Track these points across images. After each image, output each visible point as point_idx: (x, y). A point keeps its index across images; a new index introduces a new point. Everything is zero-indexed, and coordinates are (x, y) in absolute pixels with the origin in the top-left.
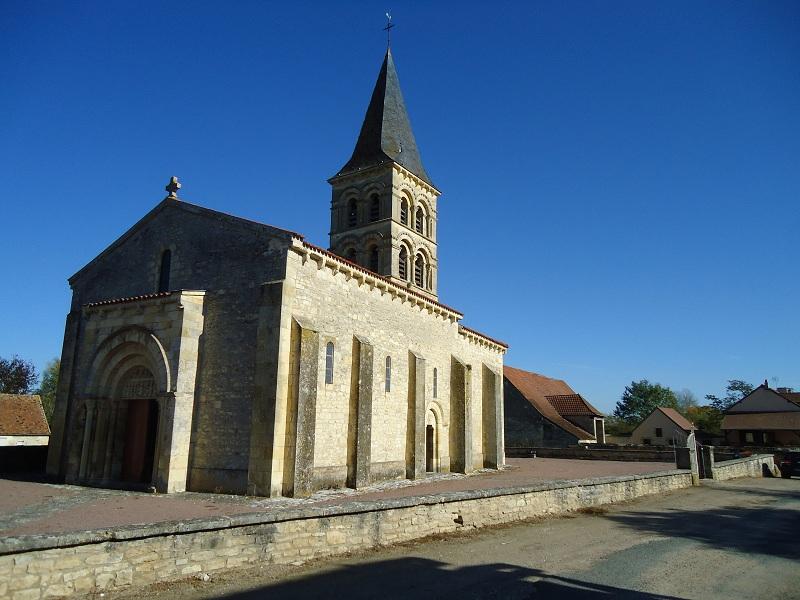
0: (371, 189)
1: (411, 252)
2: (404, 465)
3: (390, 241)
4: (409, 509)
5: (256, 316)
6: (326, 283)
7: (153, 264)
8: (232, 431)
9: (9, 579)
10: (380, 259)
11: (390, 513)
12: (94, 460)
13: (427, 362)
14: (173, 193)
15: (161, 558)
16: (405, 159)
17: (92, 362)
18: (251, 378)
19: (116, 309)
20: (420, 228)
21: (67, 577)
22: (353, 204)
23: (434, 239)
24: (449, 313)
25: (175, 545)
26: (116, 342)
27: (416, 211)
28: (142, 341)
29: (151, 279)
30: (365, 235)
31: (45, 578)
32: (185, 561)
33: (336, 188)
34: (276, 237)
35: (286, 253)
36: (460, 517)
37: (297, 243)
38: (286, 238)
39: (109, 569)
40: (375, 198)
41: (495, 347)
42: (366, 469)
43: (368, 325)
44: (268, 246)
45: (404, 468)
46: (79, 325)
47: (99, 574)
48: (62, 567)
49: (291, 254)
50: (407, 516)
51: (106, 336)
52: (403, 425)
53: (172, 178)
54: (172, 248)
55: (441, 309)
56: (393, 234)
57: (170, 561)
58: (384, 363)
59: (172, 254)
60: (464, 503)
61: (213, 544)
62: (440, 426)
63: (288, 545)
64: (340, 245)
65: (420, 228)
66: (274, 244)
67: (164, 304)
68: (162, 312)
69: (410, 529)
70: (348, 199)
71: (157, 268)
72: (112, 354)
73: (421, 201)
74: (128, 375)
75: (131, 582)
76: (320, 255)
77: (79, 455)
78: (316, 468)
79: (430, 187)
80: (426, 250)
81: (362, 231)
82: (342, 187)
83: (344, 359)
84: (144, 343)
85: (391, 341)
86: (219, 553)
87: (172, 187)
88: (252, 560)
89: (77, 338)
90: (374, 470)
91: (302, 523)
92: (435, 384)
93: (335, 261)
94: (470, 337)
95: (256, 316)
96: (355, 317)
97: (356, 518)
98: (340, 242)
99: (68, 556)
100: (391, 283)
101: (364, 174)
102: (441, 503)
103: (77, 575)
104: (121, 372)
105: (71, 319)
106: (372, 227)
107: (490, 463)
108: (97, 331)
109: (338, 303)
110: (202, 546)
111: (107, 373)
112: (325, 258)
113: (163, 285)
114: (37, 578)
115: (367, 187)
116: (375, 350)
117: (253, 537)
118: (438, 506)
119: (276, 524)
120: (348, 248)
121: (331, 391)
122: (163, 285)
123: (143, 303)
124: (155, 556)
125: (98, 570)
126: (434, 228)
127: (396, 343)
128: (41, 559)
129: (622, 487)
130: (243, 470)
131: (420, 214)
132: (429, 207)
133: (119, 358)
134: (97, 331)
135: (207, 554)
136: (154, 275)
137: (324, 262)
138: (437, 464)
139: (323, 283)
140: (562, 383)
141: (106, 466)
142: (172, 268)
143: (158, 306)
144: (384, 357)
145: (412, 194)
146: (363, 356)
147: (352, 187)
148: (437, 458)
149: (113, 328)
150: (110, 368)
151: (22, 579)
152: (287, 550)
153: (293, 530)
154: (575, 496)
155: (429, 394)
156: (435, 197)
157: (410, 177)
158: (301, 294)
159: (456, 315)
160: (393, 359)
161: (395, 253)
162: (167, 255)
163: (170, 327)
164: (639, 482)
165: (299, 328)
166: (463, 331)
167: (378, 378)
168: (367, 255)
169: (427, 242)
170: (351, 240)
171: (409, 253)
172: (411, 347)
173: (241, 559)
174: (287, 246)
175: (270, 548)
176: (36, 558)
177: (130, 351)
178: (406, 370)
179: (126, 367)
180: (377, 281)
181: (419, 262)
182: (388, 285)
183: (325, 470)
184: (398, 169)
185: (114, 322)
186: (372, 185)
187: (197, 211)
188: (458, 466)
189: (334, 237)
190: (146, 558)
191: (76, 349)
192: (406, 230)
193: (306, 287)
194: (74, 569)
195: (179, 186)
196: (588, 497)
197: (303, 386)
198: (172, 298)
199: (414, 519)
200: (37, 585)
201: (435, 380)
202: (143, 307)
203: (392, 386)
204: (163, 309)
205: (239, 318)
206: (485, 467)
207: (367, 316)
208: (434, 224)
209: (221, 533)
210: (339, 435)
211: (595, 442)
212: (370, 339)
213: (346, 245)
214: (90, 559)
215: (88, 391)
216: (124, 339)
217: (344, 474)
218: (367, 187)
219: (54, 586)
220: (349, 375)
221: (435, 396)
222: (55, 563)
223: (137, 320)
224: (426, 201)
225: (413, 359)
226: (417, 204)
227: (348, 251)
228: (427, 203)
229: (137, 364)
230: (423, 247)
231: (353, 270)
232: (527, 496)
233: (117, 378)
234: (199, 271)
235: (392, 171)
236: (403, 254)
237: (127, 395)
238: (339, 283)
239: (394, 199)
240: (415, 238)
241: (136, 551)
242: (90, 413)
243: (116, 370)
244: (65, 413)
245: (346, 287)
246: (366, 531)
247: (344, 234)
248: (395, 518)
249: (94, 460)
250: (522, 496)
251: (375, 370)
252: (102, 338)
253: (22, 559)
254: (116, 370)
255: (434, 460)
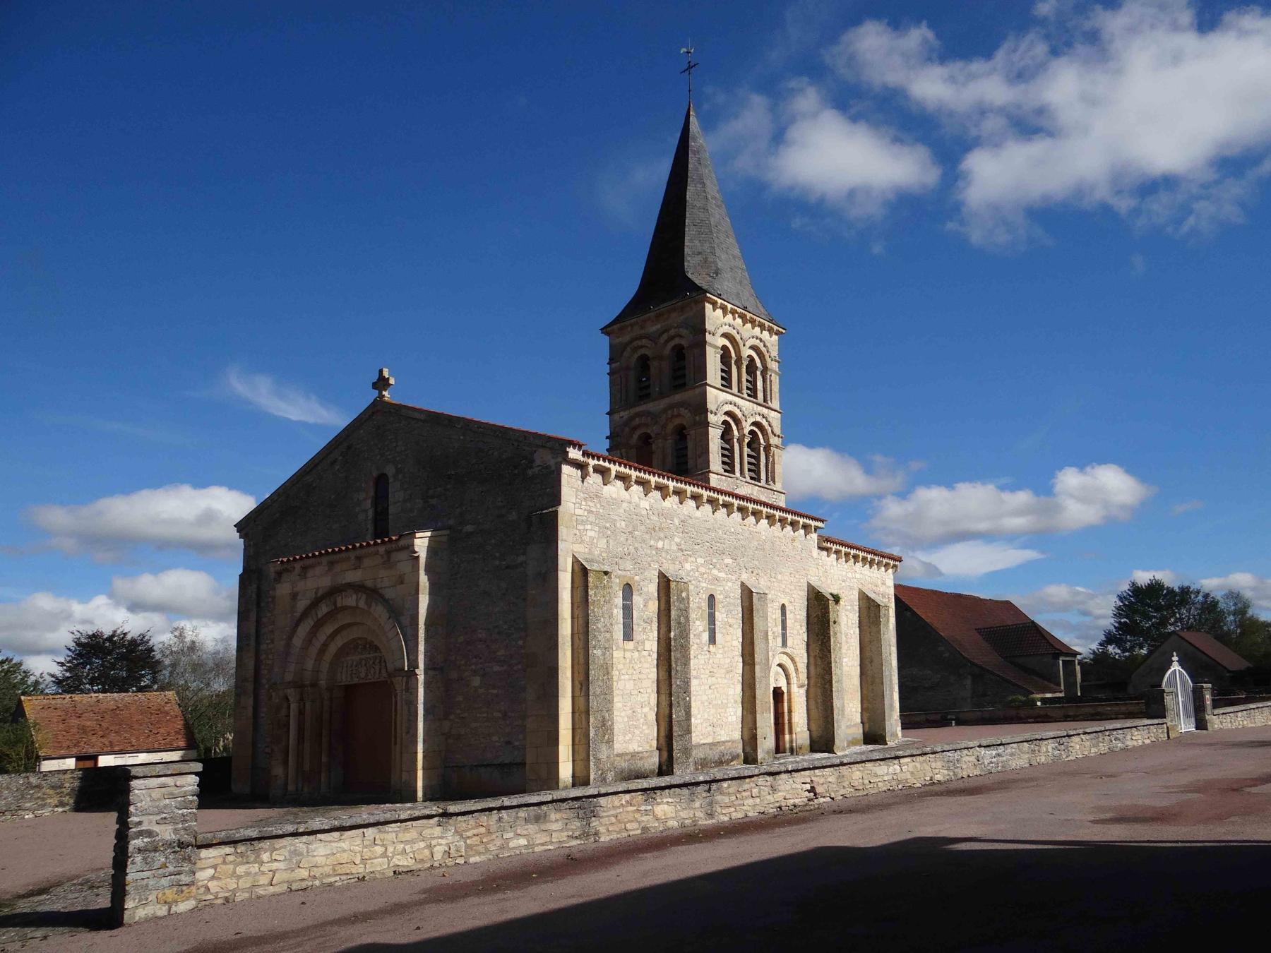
0: (672, 338)
1: (740, 429)
2: (740, 746)
3: (706, 417)
4: (747, 780)
5: (522, 558)
6: (616, 503)
7: (362, 496)
8: (500, 715)
9: (361, 849)
10: (690, 445)
11: (725, 784)
12: (307, 767)
13: (769, 596)
14: (385, 393)
15: (489, 832)
16: (726, 284)
17: (290, 638)
18: (520, 643)
19: (319, 564)
20: (753, 393)
21: (408, 848)
22: (644, 362)
23: (775, 404)
24: (802, 521)
25: (500, 819)
26: (324, 609)
27: (745, 363)
28: (362, 604)
29: (361, 517)
30: (665, 410)
31: (390, 849)
32: (511, 835)
33: (618, 341)
34: (543, 447)
35: (559, 472)
36: (813, 788)
37: (574, 454)
38: (558, 447)
39: (443, 842)
40: (679, 352)
41: (872, 560)
42: (687, 751)
43: (680, 554)
44: (532, 461)
45: (739, 749)
46: (259, 588)
47: (435, 846)
48: (403, 840)
49: (566, 469)
50: (746, 787)
51: (308, 602)
52: (735, 691)
53: (381, 371)
54: (390, 470)
55: (790, 517)
56: (708, 327)
57: (497, 834)
58: (705, 605)
59: (391, 480)
60: (817, 771)
61: (538, 819)
62: (794, 688)
63: (613, 820)
64: (627, 429)
65: (753, 393)
66: (543, 457)
67: (388, 553)
68: (388, 562)
69: (750, 801)
70: (636, 356)
71: (369, 501)
72: (319, 624)
73: (753, 348)
74: (343, 652)
75: (463, 854)
76: (607, 464)
77: (285, 762)
78: (618, 755)
79: (767, 324)
80: (764, 422)
81: (663, 403)
82: (626, 338)
83: (646, 605)
84: (366, 608)
85: (715, 572)
86: (543, 827)
87: (381, 383)
88: (577, 834)
89: (258, 604)
90: (698, 754)
91: (627, 797)
92: (784, 627)
93: (627, 471)
94: (837, 552)
95: (522, 558)
96: (660, 544)
97: (685, 791)
98: (627, 423)
99: (406, 829)
100: (710, 489)
101: (658, 316)
102: (787, 772)
103: (416, 846)
104: (333, 649)
105: (244, 580)
106: (677, 397)
107: (873, 736)
108: (294, 596)
109: (635, 528)
110: (527, 821)
111: (313, 651)
112: (614, 468)
113: (381, 530)
114: (383, 849)
115: (665, 336)
116: (691, 587)
117: (576, 811)
118: (784, 776)
119: (599, 799)
120: (638, 433)
121: (632, 651)
122: (381, 530)
123: (358, 553)
124: (482, 830)
125: (434, 842)
126: (776, 388)
127: (722, 575)
128: (385, 832)
129: (1049, 747)
130: (520, 764)
131: (751, 368)
132: (767, 356)
133: (329, 629)
134: (294, 596)
135: (532, 828)
136: (366, 511)
137: (613, 474)
138: (791, 741)
139: (615, 503)
140: (1008, 605)
141: (323, 775)
142: (391, 500)
143: (382, 556)
144: (705, 597)
145: (738, 337)
146: (673, 598)
147: (640, 338)
148: (791, 732)
149: (318, 589)
150: (317, 644)
151: (372, 849)
152: (612, 824)
153: (617, 803)
154: (973, 759)
155: (774, 642)
156: (775, 338)
157: (733, 312)
158: (583, 523)
159: (813, 523)
160: (718, 597)
161: (715, 435)
162: (381, 483)
163: (402, 583)
164: (1076, 739)
165: (585, 571)
166: (825, 544)
167: (698, 627)
168: (670, 442)
169: (765, 411)
170: (643, 420)
171: (736, 432)
172: (745, 577)
173: (566, 834)
174: (560, 459)
175: (595, 823)
176: (380, 831)
177: (345, 619)
178: (738, 612)
179: (339, 642)
180: (690, 489)
181: (753, 444)
182: (705, 493)
183: (627, 758)
184: (714, 304)
185: (319, 580)
186: (672, 332)
187: (422, 417)
188: (823, 741)
189: (616, 417)
190: (475, 832)
191: (258, 622)
192: (730, 397)
193: (590, 512)
194: (413, 842)
195: (392, 381)
196: (994, 760)
197: (594, 648)
198: (402, 543)
199: (754, 791)
200: (384, 855)
201: (784, 623)
202: (359, 558)
203: (719, 637)
204: (389, 558)
205: (497, 563)
206: (774, 688)
207: (677, 540)
208: (775, 379)
209: (544, 808)
210: (646, 710)
211: (1062, 695)
212: (683, 573)
213: (635, 428)
214: (427, 832)
215: (289, 677)
216: (335, 604)
217: (653, 761)
218: (665, 336)
219: (397, 857)
220: (655, 626)
221: (784, 643)
222: (397, 835)
223: (352, 577)
224: (761, 346)
225: (747, 595)
226: (747, 352)
227: (640, 437)
228: (764, 350)
229: (355, 636)
230: (759, 419)
231: (653, 479)
232: (902, 761)
233: (328, 656)
234: (433, 501)
235: (704, 308)
236: (726, 435)
237: (344, 678)
238: (635, 499)
239: (710, 351)
240: (748, 410)
241: (464, 825)
242: (294, 706)
243: (325, 646)
244: (250, 709)
245: (645, 504)
246: (697, 804)
247: (633, 411)
248: (731, 790)
249: (307, 767)
250: (896, 761)
251: (692, 616)
252: (302, 604)
253: (370, 832)
254: (325, 646)
255: (787, 737)
